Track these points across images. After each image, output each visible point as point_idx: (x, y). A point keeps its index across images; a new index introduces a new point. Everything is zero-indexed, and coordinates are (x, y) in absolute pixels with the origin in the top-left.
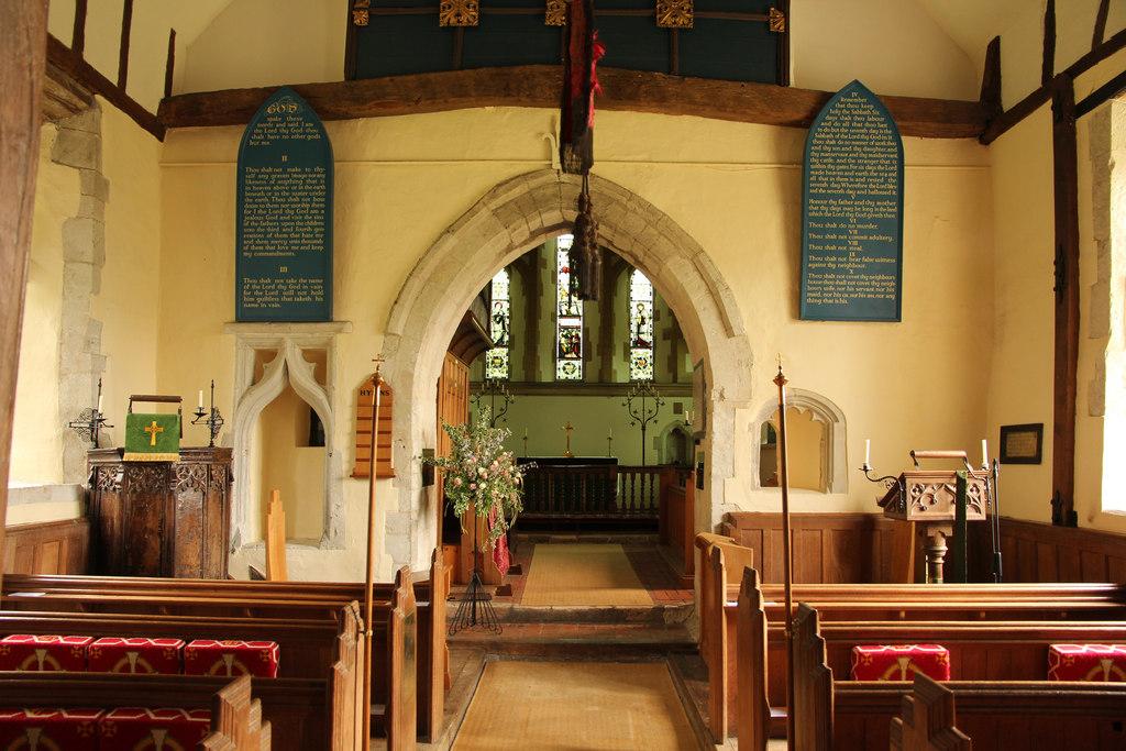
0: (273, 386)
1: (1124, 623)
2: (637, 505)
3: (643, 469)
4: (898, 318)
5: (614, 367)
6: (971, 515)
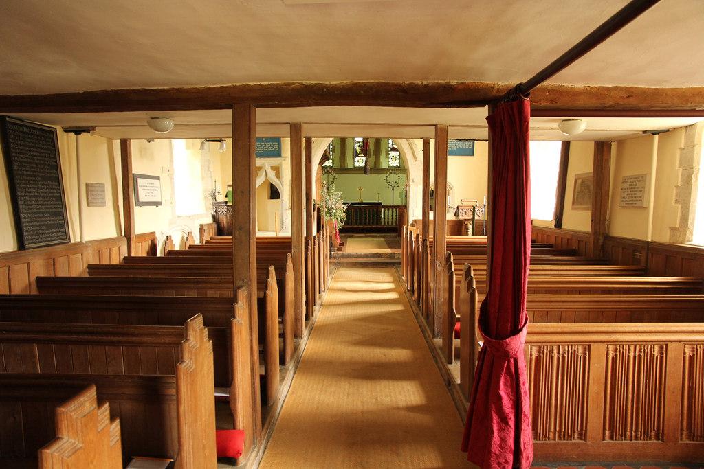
2: (390, 223)
3: (393, 207)
4: (473, 155)
5: (381, 160)
6: (476, 217)
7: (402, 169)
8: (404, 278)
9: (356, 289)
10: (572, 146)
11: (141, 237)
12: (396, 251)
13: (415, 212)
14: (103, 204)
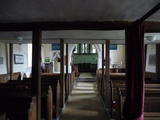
0: (55, 56)
1: (159, 85)
2: (93, 68)
4: (117, 49)
7: (96, 54)
8: (97, 86)
9: (84, 88)
10: (148, 45)
11: (16, 74)
12: (95, 77)
13: (100, 66)
14: (2, 63)
